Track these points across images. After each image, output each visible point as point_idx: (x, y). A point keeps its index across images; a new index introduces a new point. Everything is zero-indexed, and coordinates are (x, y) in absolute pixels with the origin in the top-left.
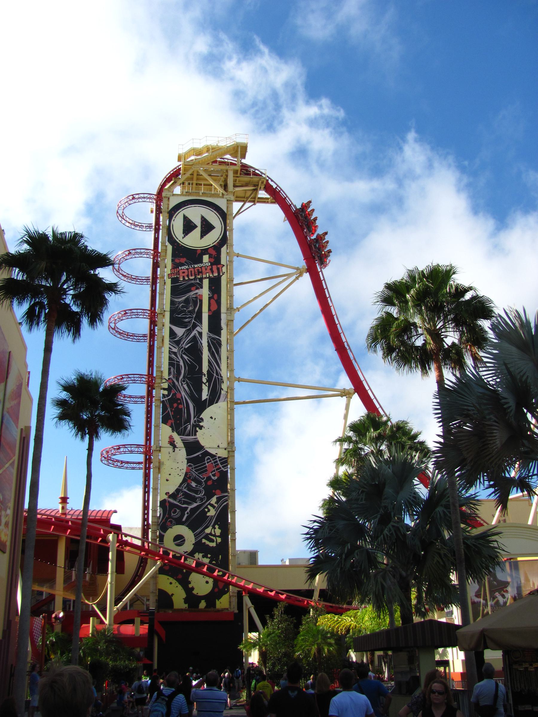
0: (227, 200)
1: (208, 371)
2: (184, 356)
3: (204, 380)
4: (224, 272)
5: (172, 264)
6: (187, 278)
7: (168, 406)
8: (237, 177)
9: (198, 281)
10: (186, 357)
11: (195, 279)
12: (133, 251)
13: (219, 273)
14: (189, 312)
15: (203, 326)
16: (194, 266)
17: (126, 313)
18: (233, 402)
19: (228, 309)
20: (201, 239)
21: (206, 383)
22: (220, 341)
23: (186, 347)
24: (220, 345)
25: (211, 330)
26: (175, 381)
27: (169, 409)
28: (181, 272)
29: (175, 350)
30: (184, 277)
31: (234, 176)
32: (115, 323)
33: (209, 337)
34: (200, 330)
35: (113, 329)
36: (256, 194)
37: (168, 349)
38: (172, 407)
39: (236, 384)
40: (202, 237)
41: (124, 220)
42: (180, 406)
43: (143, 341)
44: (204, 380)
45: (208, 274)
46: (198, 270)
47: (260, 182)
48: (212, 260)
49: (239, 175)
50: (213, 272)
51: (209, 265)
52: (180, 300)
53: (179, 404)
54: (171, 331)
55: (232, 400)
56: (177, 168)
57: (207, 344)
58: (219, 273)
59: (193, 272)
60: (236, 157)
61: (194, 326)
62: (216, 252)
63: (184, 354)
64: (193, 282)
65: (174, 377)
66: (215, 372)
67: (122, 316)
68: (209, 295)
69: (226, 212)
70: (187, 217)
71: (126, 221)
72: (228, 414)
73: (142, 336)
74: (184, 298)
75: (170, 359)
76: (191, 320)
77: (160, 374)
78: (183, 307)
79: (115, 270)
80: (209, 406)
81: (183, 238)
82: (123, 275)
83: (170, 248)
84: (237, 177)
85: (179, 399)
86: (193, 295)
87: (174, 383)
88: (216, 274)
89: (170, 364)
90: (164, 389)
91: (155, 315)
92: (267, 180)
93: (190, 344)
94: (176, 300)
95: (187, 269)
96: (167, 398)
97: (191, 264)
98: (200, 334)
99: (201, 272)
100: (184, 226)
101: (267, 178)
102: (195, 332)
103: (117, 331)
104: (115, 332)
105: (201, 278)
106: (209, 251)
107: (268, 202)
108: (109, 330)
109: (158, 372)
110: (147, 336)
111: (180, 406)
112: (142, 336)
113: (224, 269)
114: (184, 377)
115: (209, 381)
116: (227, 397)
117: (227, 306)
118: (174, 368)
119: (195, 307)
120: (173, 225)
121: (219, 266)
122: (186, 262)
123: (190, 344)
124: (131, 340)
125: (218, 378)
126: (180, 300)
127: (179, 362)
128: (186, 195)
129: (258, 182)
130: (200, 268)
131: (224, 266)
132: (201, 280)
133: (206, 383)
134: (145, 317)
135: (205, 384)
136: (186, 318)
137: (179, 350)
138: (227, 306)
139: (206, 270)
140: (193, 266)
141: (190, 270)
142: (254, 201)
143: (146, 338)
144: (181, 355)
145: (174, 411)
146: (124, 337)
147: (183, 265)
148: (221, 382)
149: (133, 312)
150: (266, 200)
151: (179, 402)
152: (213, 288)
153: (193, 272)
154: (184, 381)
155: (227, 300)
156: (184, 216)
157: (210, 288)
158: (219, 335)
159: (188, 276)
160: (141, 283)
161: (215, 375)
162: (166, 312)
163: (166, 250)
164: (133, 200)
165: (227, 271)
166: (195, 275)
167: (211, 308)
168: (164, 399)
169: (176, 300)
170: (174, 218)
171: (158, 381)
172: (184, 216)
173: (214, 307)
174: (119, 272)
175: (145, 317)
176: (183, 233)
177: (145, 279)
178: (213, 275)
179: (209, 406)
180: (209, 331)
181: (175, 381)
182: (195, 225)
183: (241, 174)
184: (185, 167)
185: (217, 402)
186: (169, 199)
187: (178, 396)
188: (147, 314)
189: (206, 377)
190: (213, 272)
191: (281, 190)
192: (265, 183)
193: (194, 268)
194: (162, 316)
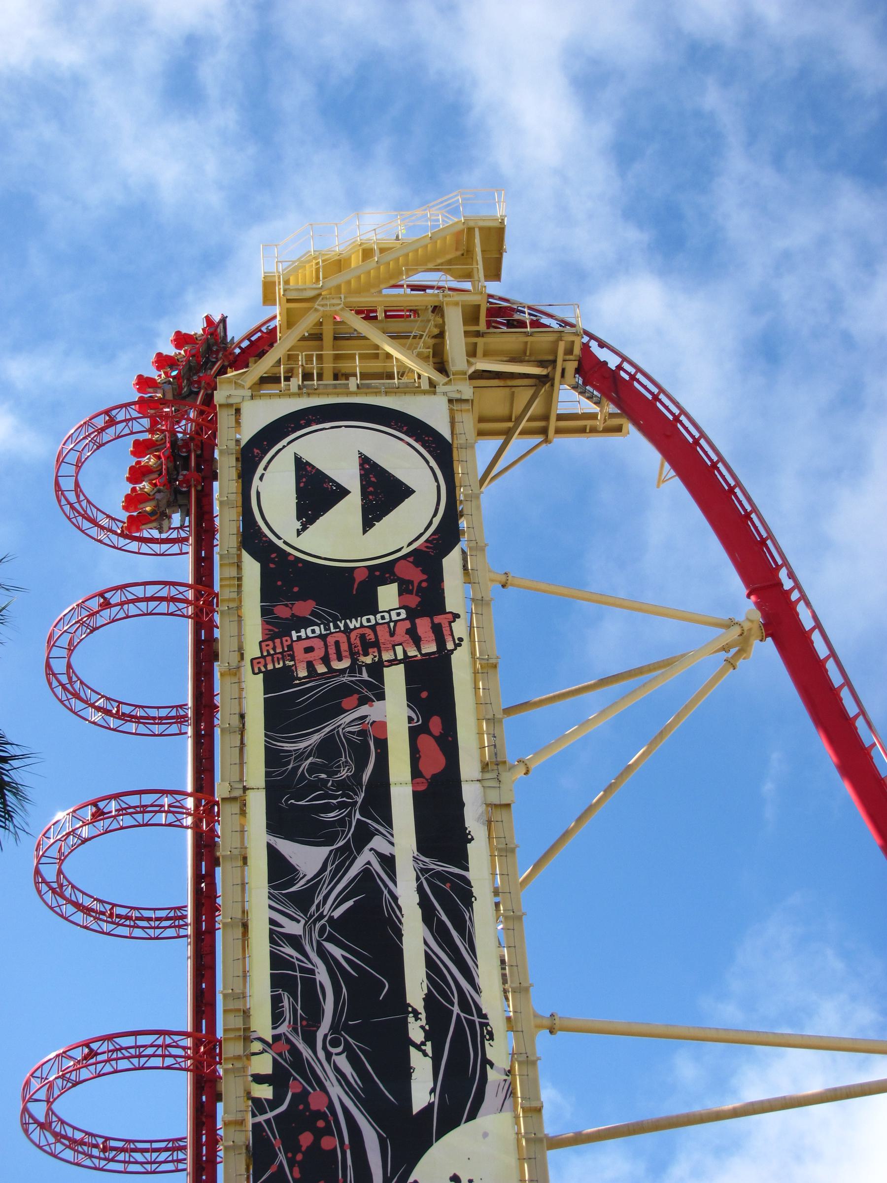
0: (450, 401)
1: (429, 1000)
2: (331, 947)
3: (416, 1032)
4: (461, 639)
5: (265, 622)
6: (321, 669)
7: (277, 1143)
8: (478, 334)
9: (365, 676)
10: (337, 952)
11: (354, 668)
12: (113, 806)
13: (441, 642)
14: (341, 785)
15: (395, 832)
16: (346, 625)
17: (93, 1054)
18: (540, 1140)
19: (485, 767)
20: (365, 532)
21: (423, 1044)
22: (468, 883)
23: (337, 914)
24: (467, 896)
25: (425, 845)
26: (301, 1046)
27: (282, 1157)
28: (299, 648)
29: (294, 928)
30: (310, 666)
31: (467, 334)
32: (48, 1101)
33: (424, 871)
34: (385, 849)
35: (42, 1126)
36: (549, 400)
37: (267, 926)
38: (291, 1146)
39: (543, 1042)
40: (367, 525)
41: (81, 699)
42: (327, 1143)
43: (170, 1166)
44: (416, 1032)
45: (399, 650)
46: (363, 637)
47: (562, 347)
48: (413, 601)
49: (482, 326)
50: (417, 642)
51: (403, 615)
52: (302, 745)
53: (319, 1134)
54: (275, 859)
55: (534, 1104)
56: (264, 329)
57: (416, 898)
58: (441, 642)
59: (344, 647)
60: (468, 276)
61: (363, 836)
62: (423, 572)
63: (331, 939)
64: (345, 679)
65: (295, 1030)
66: (456, 1001)
67: (80, 1065)
68: (410, 719)
69: (447, 435)
70: (307, 463)
71: (85, 702)
72: (521, 1160)
73: (166, 1149)
74: (316, 738)
75: (277, 961)
76: (349, 815)
77: (239, 1023)
78: (313, 769)
79: (44, 888)
80: (441, 1134)
81: (299, 533)
82: (78, 906)
83: (252, 569)
84: (478, 334)
85: (323, 1116)
86: (350, 724)
87: (294, 1051)
88: (430, 647)
89: (277, 982)
90: (259, 1079)
91: (211, 1052)
92: (586, 347)
93: (350, 903)
94: (287, 746)
95: (322, 637)
96: (270, 1115)
97: (335, 620)
98: (388, 862)
99: (376, 644)
100: (300, 492)
101: (586, 339)
102: (366, 857)
103: (58, 1136)
104: (52, 1140)
105: (374, 663)
106: (398, 570)
107: (594, 430)
108: (26, 1131)
109: (231, 1016)
110: (184, 1148)
111: (327, 1143)
112: (166, 1149)
113: (459, 629)
114: (334, 1028)
115: (435, 1034)
116: (511, 1092)
117: (482, 755)
118: (294, 995)
119: (361, 766)
120: (258, 494)
121: (438, 619)
122: (313, 614)
123: (350, 903)
124: (120, 1167)
125: (471, 1023)
126: (302, 745)
127: (312, 972)
128: (299, 395)
129: (555, 353)
130: (368, 631)
131: (456, 616)
132: (377, 670)
133: (423, 1044)
134: (169, 1061)
135: (418, 1047)
136: (328, 808)
137: (309, 931)
138: (482, 755)
139: (392, 634)
140: (342, 625)
141: (331, 640)
142: (544, 431)
143: (181, 1156)
144: (319, 945)
145: (301, 1164)
146: (91, 1156)
147: (305, 623)
148: (483, 1037)
149: (122, 1048)
150: (589, 423)
151: (321, 1124)
152: (424, 695)
153: (344, 647)
154: (335, 1043)
155: (480, 734)
156: (298, 461)
157: (412, 697)
158: (462, 860)
159: (326, 660)
160: (151, 932)
161: (456, 1009)
162: (250, 793)
163: (240, 579)
164: (106, 613)
165: (471, 634)
166: (353, 656)
167: (422, 766)
168: (261, 1118)
169: (287, 746)
170: (260, 470)
171: (232, 1049)
172: (298, 461)
173: (434, 763)
174: (63, 896)
175: (169, 1061)
176: (299, 518)
177: (167, 918)
178: (419, 650)
179: (442, 1132)
180: (419, 849)
181: (301, 1046)
182: (339, 486)
183: (489, 325)
184: (288, 310)
185: (472, 1116)
186: (238, 411)
187: (316, 1102)
188: (180, 1052)
189: (423, 1022)
190: (417, 642)
191: (639, 370)
192: (577, 350)
193: (347, 631)
194: (235, 808)
